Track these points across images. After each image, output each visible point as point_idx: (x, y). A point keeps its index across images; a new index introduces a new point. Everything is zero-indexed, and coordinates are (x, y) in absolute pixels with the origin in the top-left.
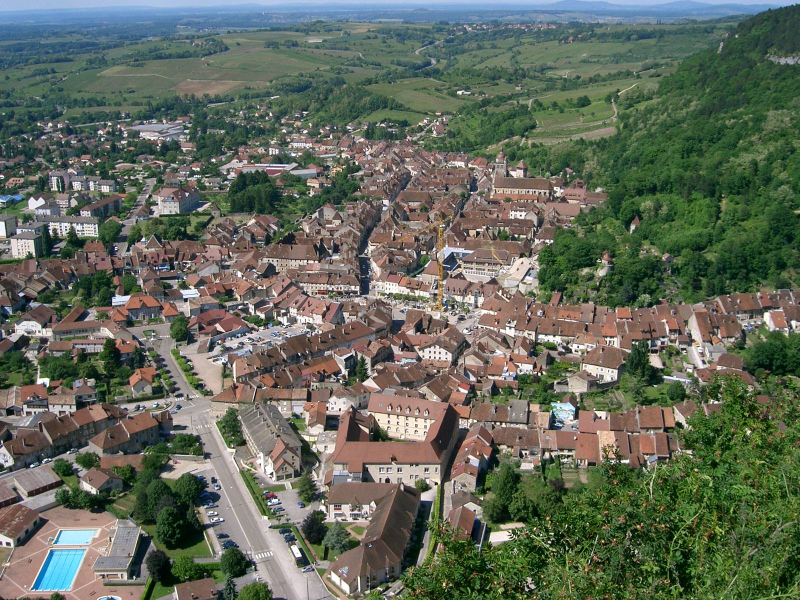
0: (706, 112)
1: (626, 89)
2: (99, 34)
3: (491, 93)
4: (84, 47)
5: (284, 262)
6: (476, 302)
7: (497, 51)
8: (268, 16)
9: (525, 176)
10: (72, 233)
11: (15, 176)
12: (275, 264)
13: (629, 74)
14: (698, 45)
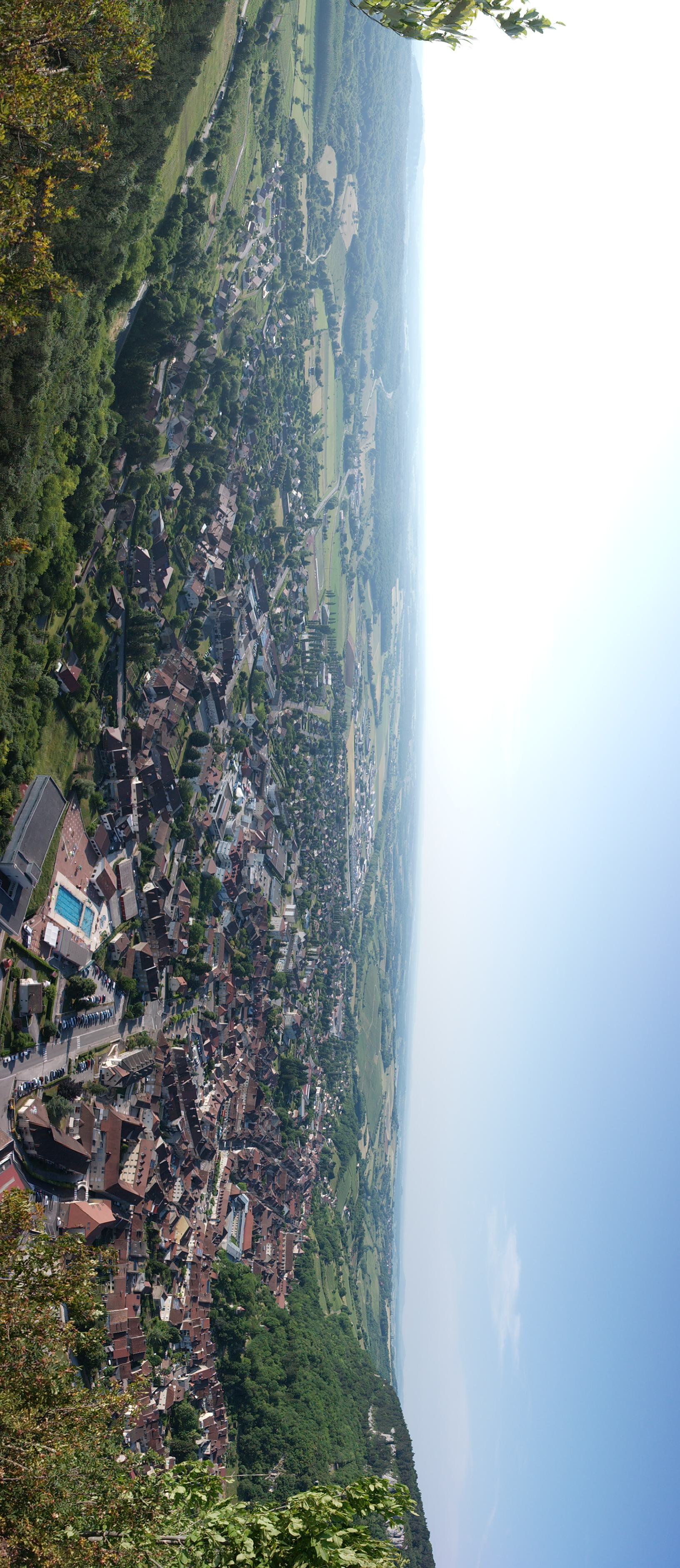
0: (338, 1369)
1: (353, 1320)
2: (400, 990)
3: (349, 1233)
4: (394, 980)
10: (280, 956)
14: (378, 1362)
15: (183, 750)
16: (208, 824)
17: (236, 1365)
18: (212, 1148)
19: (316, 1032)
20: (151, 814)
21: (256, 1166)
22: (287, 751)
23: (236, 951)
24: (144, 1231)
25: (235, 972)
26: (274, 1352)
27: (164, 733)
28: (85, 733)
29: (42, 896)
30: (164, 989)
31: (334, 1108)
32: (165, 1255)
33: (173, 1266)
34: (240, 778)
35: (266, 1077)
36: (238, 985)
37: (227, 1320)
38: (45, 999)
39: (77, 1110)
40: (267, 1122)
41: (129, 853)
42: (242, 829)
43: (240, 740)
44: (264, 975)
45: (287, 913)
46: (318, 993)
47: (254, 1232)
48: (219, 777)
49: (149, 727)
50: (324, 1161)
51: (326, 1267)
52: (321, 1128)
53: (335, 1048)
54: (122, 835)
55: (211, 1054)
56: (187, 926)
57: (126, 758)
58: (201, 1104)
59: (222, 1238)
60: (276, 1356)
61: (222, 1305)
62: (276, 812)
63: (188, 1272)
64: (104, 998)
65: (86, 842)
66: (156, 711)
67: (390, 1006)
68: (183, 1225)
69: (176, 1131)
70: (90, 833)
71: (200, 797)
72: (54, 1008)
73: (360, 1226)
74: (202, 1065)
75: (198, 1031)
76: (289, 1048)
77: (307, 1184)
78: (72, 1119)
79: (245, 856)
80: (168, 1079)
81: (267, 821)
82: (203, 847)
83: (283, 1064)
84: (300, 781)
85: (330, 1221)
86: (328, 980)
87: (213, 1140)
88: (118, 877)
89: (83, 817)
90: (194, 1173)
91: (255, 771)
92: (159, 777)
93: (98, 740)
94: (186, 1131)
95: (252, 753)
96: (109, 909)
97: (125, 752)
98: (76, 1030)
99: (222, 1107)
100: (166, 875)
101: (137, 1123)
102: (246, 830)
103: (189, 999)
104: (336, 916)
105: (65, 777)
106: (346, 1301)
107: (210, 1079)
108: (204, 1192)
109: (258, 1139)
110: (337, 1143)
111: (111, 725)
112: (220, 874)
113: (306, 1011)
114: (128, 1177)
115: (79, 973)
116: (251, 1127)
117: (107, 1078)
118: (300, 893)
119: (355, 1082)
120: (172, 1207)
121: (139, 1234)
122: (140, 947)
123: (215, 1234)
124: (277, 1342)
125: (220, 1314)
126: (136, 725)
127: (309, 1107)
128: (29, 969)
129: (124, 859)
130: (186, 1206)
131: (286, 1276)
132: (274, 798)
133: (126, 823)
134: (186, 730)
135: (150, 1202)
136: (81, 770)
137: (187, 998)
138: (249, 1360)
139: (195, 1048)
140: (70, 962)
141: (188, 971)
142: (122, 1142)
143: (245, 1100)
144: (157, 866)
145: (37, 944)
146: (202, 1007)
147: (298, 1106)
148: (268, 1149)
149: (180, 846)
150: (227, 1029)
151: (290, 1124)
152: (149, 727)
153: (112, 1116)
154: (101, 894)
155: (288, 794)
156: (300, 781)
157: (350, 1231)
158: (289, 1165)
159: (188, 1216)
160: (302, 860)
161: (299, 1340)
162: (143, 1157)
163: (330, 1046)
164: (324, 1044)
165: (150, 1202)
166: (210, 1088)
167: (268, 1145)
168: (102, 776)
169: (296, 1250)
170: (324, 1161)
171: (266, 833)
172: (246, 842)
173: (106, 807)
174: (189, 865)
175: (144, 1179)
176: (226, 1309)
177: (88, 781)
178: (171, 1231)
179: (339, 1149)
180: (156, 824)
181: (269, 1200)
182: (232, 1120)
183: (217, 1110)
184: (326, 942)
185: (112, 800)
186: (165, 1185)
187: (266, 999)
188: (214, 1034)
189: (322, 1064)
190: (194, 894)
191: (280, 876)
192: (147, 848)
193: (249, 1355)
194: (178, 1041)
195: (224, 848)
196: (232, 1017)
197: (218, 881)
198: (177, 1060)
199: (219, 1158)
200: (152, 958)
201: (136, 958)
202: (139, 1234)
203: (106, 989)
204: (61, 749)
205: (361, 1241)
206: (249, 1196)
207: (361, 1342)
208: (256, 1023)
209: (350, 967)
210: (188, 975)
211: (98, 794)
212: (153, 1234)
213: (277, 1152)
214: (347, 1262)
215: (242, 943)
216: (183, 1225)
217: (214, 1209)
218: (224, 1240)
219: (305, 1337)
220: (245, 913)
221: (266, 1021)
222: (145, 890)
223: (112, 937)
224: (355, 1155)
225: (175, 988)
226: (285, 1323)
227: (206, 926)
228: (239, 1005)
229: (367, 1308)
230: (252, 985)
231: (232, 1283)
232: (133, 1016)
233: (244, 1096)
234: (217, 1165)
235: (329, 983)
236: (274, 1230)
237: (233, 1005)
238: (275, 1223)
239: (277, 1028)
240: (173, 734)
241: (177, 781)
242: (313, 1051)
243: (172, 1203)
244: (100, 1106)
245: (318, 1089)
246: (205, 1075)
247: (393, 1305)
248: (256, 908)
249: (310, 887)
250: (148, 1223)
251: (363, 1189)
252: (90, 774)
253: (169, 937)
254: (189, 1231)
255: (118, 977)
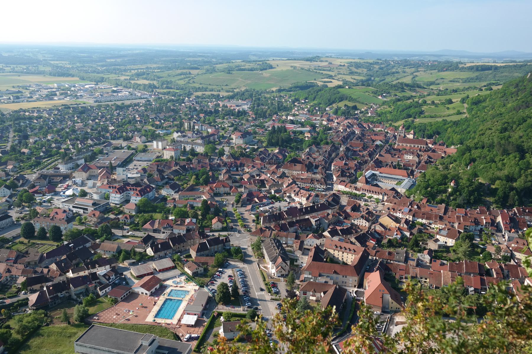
0: (517, 109)
1: (474, 94)
2: (213, 58)
3: (400, 95)
5: (290, 172)
6: (383, 198)
7: (405, 74)
8: (292, 53)
9: (414, 138)
10: (193, 150)
11: (168, 121)
12: (286, 172)
13: (475, 88)
14: (516, 75)
15: (39, 242)
16: (97, 213)
17: (500, 193)
18: (331, 196)
19: (247, 120)
20: (95, 258)
21: (345, 164)
22: (28, 159)
23: (191, 183)
24: (388, 250)
25: (206, 182)
26: (493, 161)
27: (27, 260)
28: (37, 323)
29: (163, 330)
30: (221, 233)
31: (303, 106)
32: (406, 236)
33: (415, 231)
34: (57, 194)
35: (281, 157)
36: (215, 179)
37: (460, 194)
38: (233, 319)
39: (305, 294)
40: (313, 156)
41: (127, 269)
42: (99, 187)
43: (24, 198)
44: (207, 161)
45: (160, 147)
46: (219, 120)
47: (395, 167)
48: (58, 210)
49: (24, 273)
50: (343, 113)
51: (426, 114)
52: (318, 116)
53: (258, 106)
54: (114, 277)
55: (265, 197)
56: (176, 221)
57: (52, 286)
58: (301, 204)
59: (397, 192)
60: (497, 159)
61: (448, 197)
62: (82, 161)
63: (420, 220)
64: (230, 276)
65: (122, 303)
66: (9, 271)
67: (225, 65)
68: (386, 220)
69: (319, 222)
70: (115, 302)
71: (76, 223)
72: (238, 313)
73: (395, 86)
74: (273, 203)
75: (249, 207)
76: (259, 140)
77: (360, 126)
78: (311, 298)
79: (119, 182)
80: (283, 228)
81: (89, 168)
82: (116, 215)
83: (271, 144)
84: (54, 145)
85: (390, 109)
86: (209, 113)
87: (326, 195)
88: (145, 275)
89: (103, 310)
90: (349, 210)
91: (49, 182)
92: (64, 257)
93: (41, 311)
94: (319, 215)
95: (33, 186)
96: (168, 279)
97: (48, 287)
98: (252, 295)
99: (303, 188)
100: (140, 239)
101: (314, 250)
102: (99, 184)
103: (228, 214)
104: (160, 110)
105: (74, 330)
106: (456, 99)
107: (283, 197)
108: (362, 203)
109: (326, 163)
110: (330, 103)
111: (27, 304)
112: (135, 199)
113: (232, 128)
114: (350, 258)
115: (214, 296)
116: (317, 167)
117: (284, 273)
118: (144, 138)
119: (284, 90)
120: (372, 228)
121: (390, 253)
122: (193, 253)
123: (394, 197)
124: (485, 157)
125: (455, 199)
126: (23, 284)
127: (303, 125)
128: (213, 333)
129: (131, 273)
130: (372, 217)
131: (430, 146)
132: (70, 165)
133: (104, 276)
134: (22, 243)
135: (368, 244)
136: (67, 319)
137: (226, 216)
138: (498, 182)
139: (261, 209)
140: (207, 303)
141: (208, 216)
142: (326, 262)
143: (297, 172)
144: (134, 247)
145: (197, 329)
146: (233, 205)
147: (302, 133)
148: (333, 155)
149: (117, 232)
150: (247, 186)
151: (315, 138)
152: (24, 273)
153: (309, 268)
154: (158, 286)
155: (66, 154)
156: (54, 145)
157: (398, 94)
158: (345, 140)
159: (378, 217)
160: (118, 138)
161: (485, 139)
162: (337, 247)
163: (257, 110)
164: (256, 114)
165: (368, 244)
166: (289, 197)
167: (330, 155)
168: (69, 302)
169: (411, 136)
170: (343, 113)
171: (100, 168)
172: (108, 183)
173: (93, 293)
174: (131, 224)
175: (352, 247)
176: (451, 194)
177: (75, 312)
178: (390, 230)
179: (334, 102)
180: (102, 252)
181: (371, 155)
182: (312, 181)
183: (305, 192)
184: (180, 117)
185: (87, 290)
186: (357, 232)
187: (224, 158)
188: (251, 195)
189: (270, 116)
190: (152, 217)
191: (132, 154)
192: (121, 257)
193: (493, 181)
194: (257, 221)
195: (115, 198)
196: (239, 183)
197: (141, 201)
198: (270, 222)
199: (339, 191)
200: (200, 244)
201: (201, 256)
202: (390, 253)
203: (223, 275)
204: (53, 338)
205: (407, 85)
206: (367, 170)
207: (495, 88)
208: (242, 165)
209: (198, 97)
210: (211, 216)
211: (84, 302)
212: (391, 244)
213: (335, 149)
214: (424, 96)
215: (184, 179)
216: (386, 220)
217: (375, 196)
218: (399, 190)
219: (483, 134)
220: (163, 178)
221: (240, 158)
222: (153, 254)
223: (187, 275)
224: (340, 90)
225: (220, 225)
226: (469, 149)
227: (175, 206)
228: (230, 178)
229: (465, 82)
230: (215, 169)
231: (432, 188)
232: (240, 255)
233: (295, 173)
234: (344, 193)
235: (211, 112)
236: (393, 152)
237: (230, 182)
238: (388, 152)
239: (245, 149)
240: (27, 253)
241: (66, 243)
242: (261, 123)
243: (370, 228)
244: (302, 277)
245: (290, 118)
246: (280, 201)
247: (466, 60)
248: (158, 170)
249: (139, 131)
250: (383, 246)
251: (366, 83)
252: (69, 311)
253: (185, 232)
254: (390, 216)
255: (215, 267)
